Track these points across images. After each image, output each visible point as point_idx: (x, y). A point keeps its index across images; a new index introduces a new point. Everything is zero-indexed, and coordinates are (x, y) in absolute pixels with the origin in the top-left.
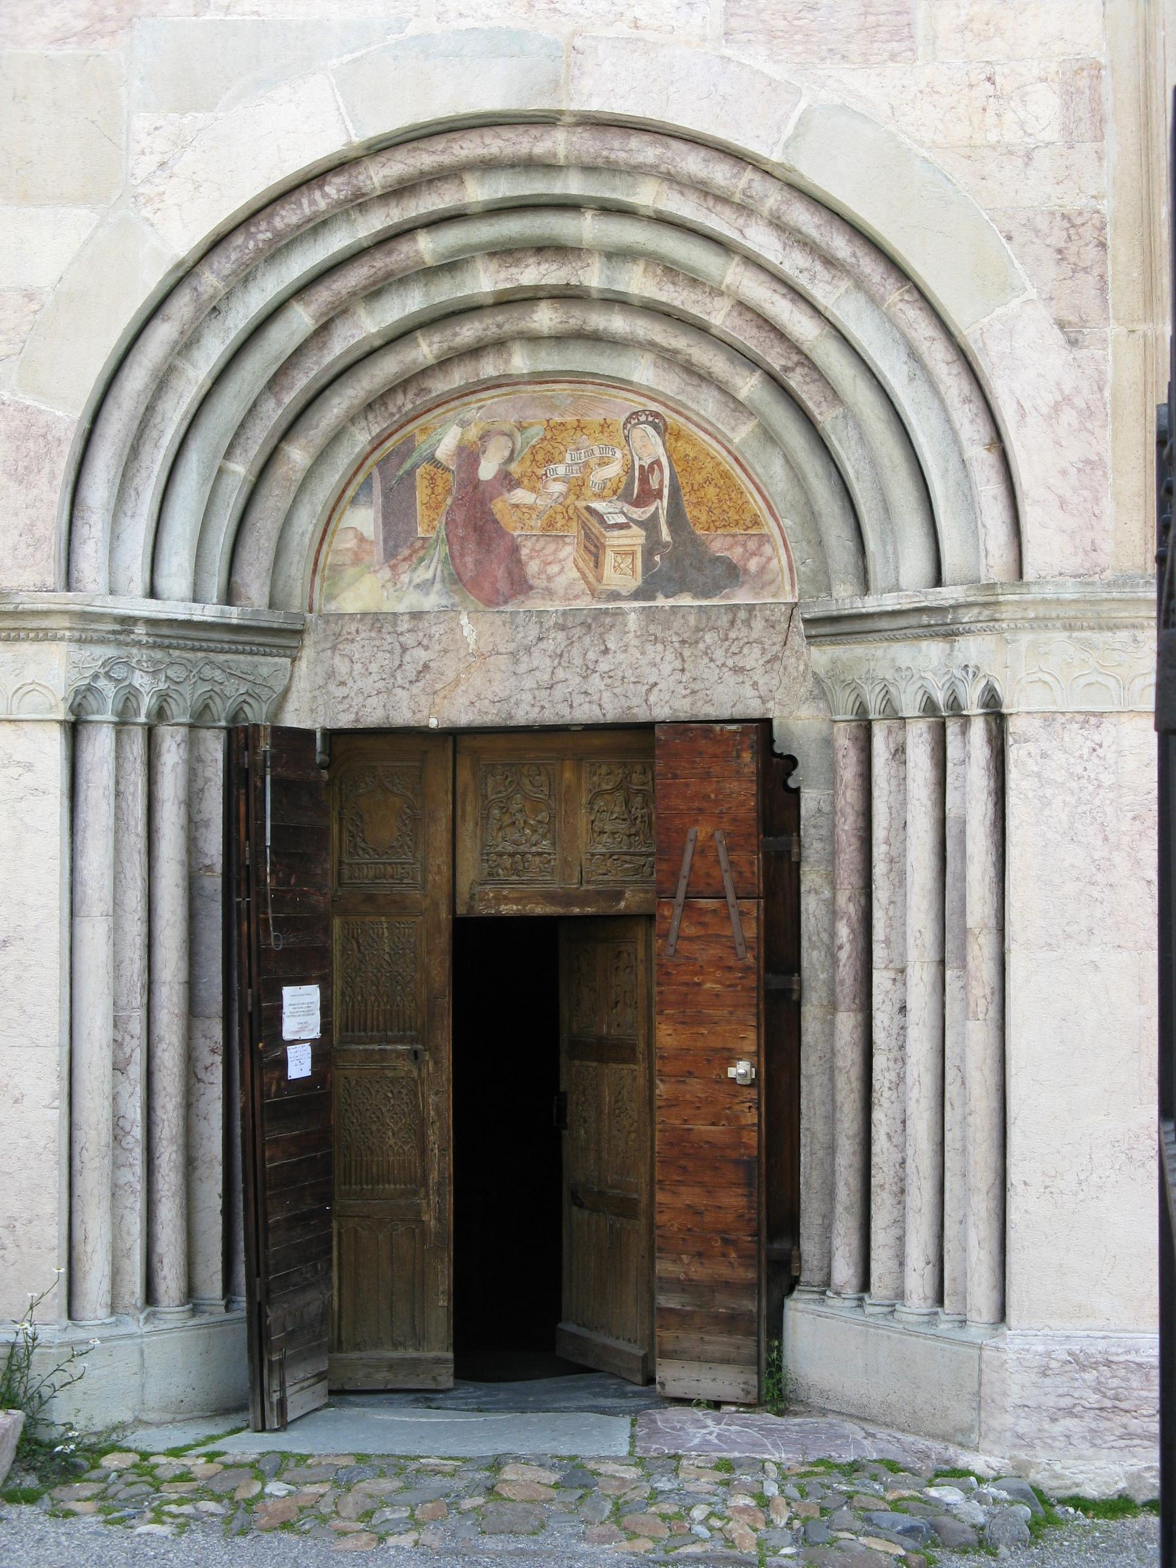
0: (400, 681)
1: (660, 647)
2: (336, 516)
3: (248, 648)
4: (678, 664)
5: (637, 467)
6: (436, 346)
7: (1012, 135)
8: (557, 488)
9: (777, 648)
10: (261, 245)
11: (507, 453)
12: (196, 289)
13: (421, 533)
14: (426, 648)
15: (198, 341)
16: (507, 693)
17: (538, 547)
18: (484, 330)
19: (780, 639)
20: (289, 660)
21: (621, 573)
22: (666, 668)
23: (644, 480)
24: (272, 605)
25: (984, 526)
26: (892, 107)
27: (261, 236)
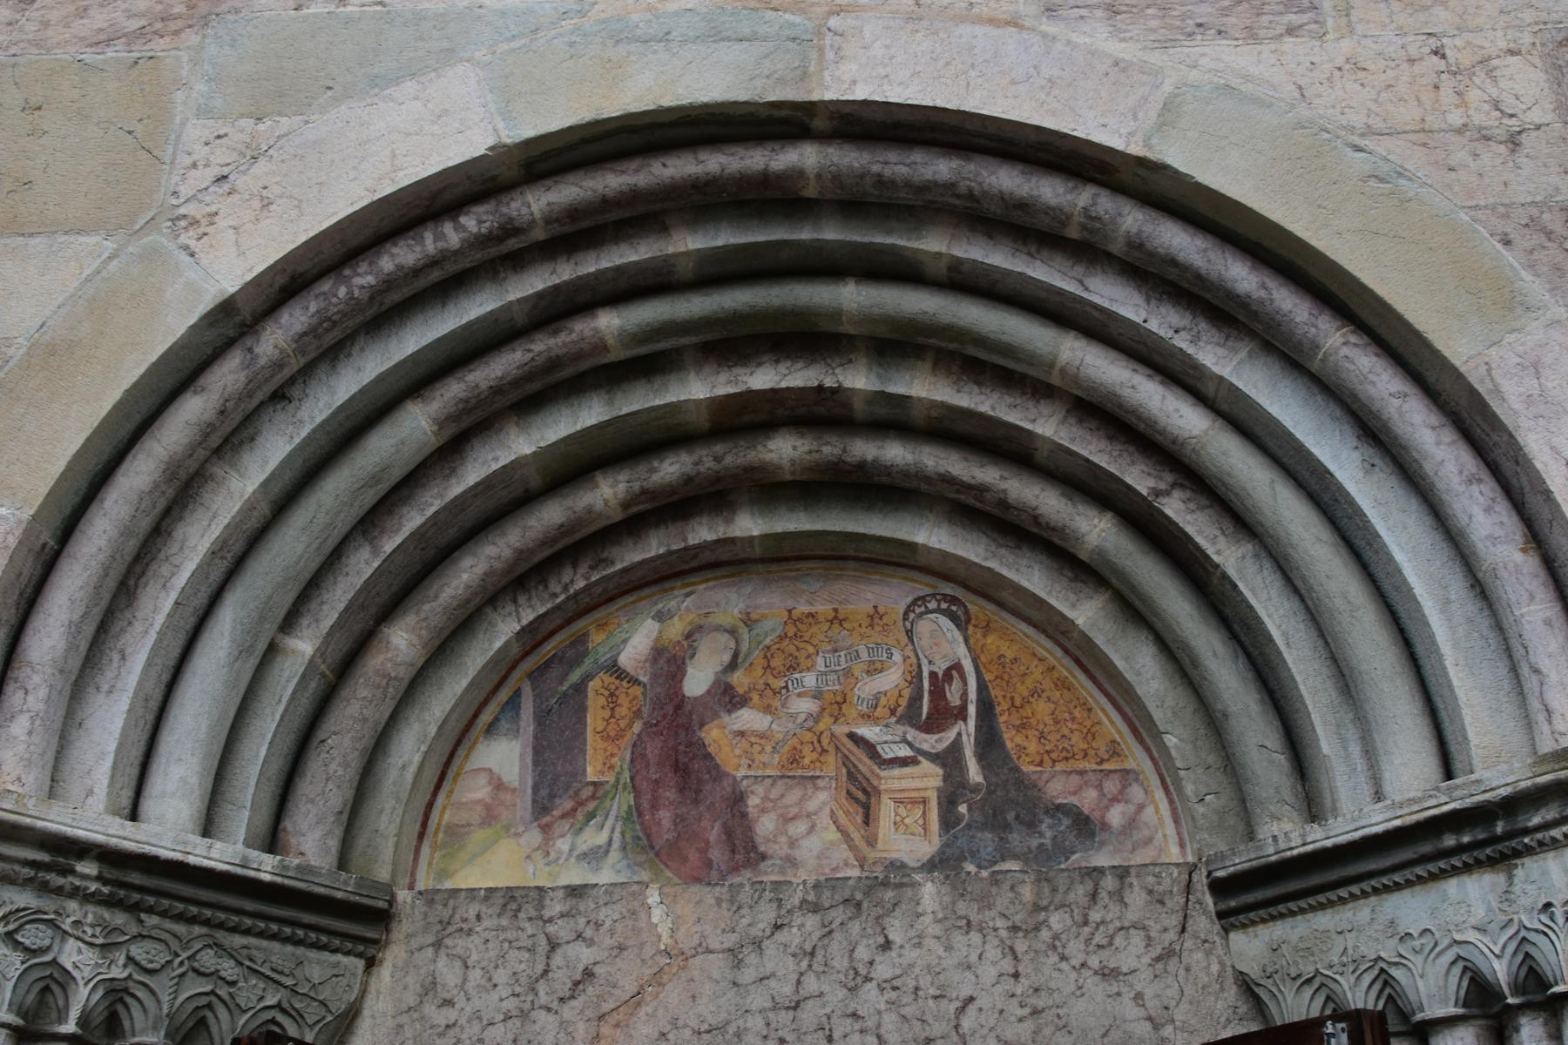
0: (543, 999)
1: (975, 937)
2: (461, 752)
3: (288, 930)
4: (1007, 965)
5: (926, 674)
6: (622, 487)
7: (1483, 117)
8: (805, 706)
9: (1172, 935)
10: (356, 293)
11: (727, 658)
12: (250, 350)
13: (591, 775)
14: (590, 943)
15: (252, 439)
16: (723, 1016)
17: (774, 794)
18: (696, 464)
19: (1174, 921)
20: (360, 964)
21: (907, 837)
22: (989, 973)
23: (938, 693)
24: (343, 863)
25: (1537, 671)
26: (1300, 88)
27: (358, 281)
